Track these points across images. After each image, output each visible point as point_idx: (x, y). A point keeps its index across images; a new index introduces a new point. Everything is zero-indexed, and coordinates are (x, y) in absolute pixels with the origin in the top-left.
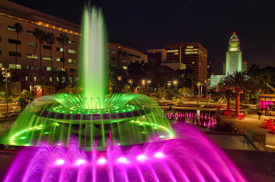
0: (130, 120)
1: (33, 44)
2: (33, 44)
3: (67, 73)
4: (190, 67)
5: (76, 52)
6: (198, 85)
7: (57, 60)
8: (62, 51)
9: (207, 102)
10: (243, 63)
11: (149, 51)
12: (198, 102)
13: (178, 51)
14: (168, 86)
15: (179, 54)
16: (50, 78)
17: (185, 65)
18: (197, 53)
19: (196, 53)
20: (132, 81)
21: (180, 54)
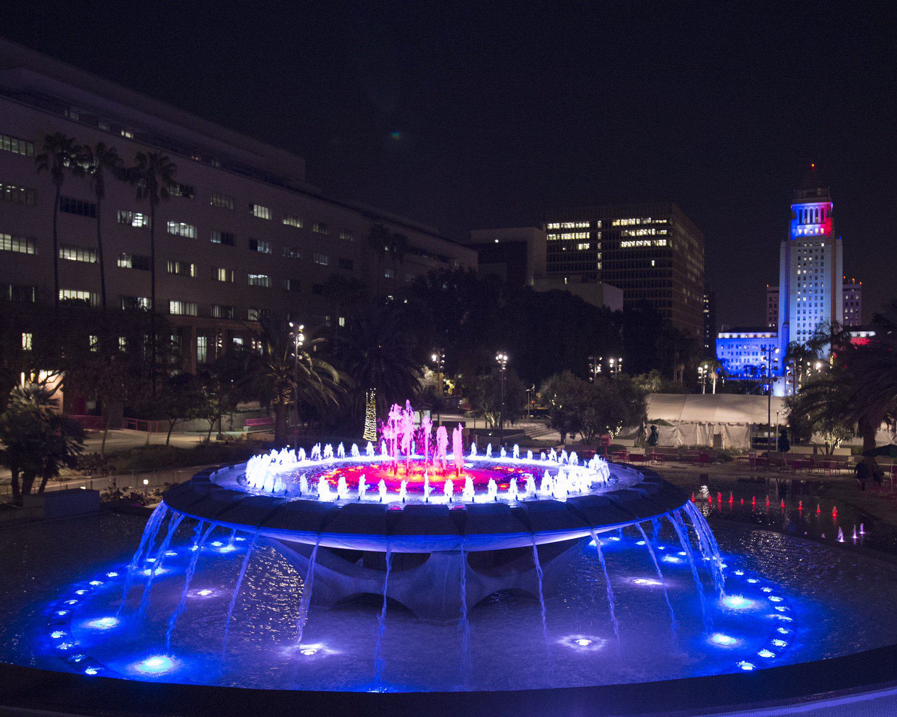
0: (589, 645)
1: (18, 190)
2: (18, 190)
3: (51, 409)
4: (648, 299)
5: (34, 495)
6: (700, 370)
7: (119, 265)
8: (140, 225)
9: (202, 347)
10: (847, 286)
11: (478, 235)
12: (840, 472)
13: (588, 237)
14: (592, 375)
15: (593, 247)
16: (91, 337)
17: (622, 291)
18: (665, 244)
19: (662, 243)
20: (612, 371)
21: (599, 246)
